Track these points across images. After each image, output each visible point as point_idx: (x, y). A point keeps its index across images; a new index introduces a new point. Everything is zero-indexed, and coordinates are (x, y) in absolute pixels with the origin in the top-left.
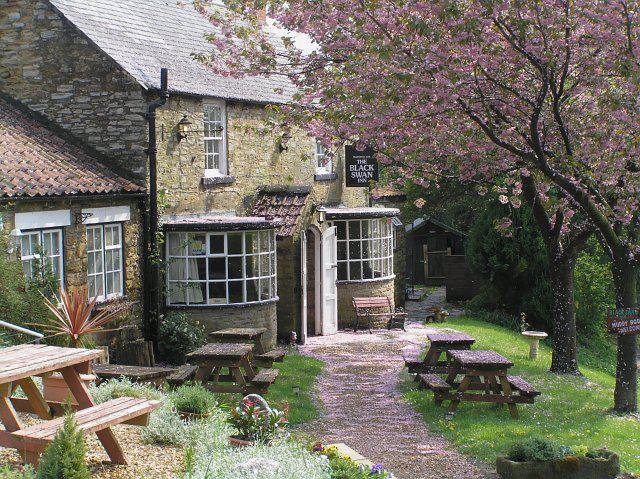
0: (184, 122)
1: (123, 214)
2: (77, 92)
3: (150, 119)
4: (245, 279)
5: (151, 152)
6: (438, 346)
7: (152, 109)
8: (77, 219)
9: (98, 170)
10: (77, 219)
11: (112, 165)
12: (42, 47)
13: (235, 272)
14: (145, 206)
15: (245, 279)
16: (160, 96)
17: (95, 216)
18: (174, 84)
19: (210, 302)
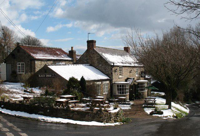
0: (116, 69)
1: (108, 82)
2: (102, 65)
3: (112, 69)
4: (124, 88)
5: (112, 73)
6: (157, 93)
7: (112, 68)
8: (102, 83)
9: (109, 61)
10: (102, 83)
11: (107, 75)
12: (97, 59)
13: (123, 90)
14: (111, 80)
15: (124, 91)
16: (114, 66)
17: (104, 82)
18: (115, 65)
19: (120, 94)
